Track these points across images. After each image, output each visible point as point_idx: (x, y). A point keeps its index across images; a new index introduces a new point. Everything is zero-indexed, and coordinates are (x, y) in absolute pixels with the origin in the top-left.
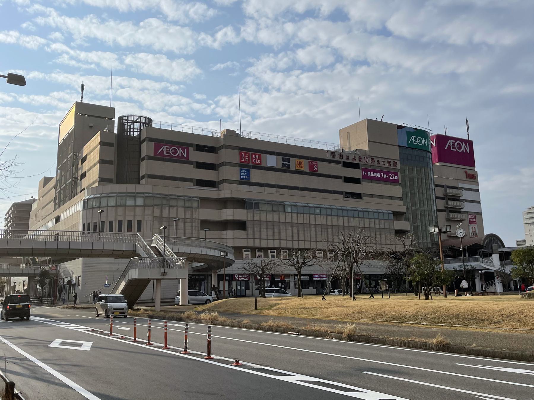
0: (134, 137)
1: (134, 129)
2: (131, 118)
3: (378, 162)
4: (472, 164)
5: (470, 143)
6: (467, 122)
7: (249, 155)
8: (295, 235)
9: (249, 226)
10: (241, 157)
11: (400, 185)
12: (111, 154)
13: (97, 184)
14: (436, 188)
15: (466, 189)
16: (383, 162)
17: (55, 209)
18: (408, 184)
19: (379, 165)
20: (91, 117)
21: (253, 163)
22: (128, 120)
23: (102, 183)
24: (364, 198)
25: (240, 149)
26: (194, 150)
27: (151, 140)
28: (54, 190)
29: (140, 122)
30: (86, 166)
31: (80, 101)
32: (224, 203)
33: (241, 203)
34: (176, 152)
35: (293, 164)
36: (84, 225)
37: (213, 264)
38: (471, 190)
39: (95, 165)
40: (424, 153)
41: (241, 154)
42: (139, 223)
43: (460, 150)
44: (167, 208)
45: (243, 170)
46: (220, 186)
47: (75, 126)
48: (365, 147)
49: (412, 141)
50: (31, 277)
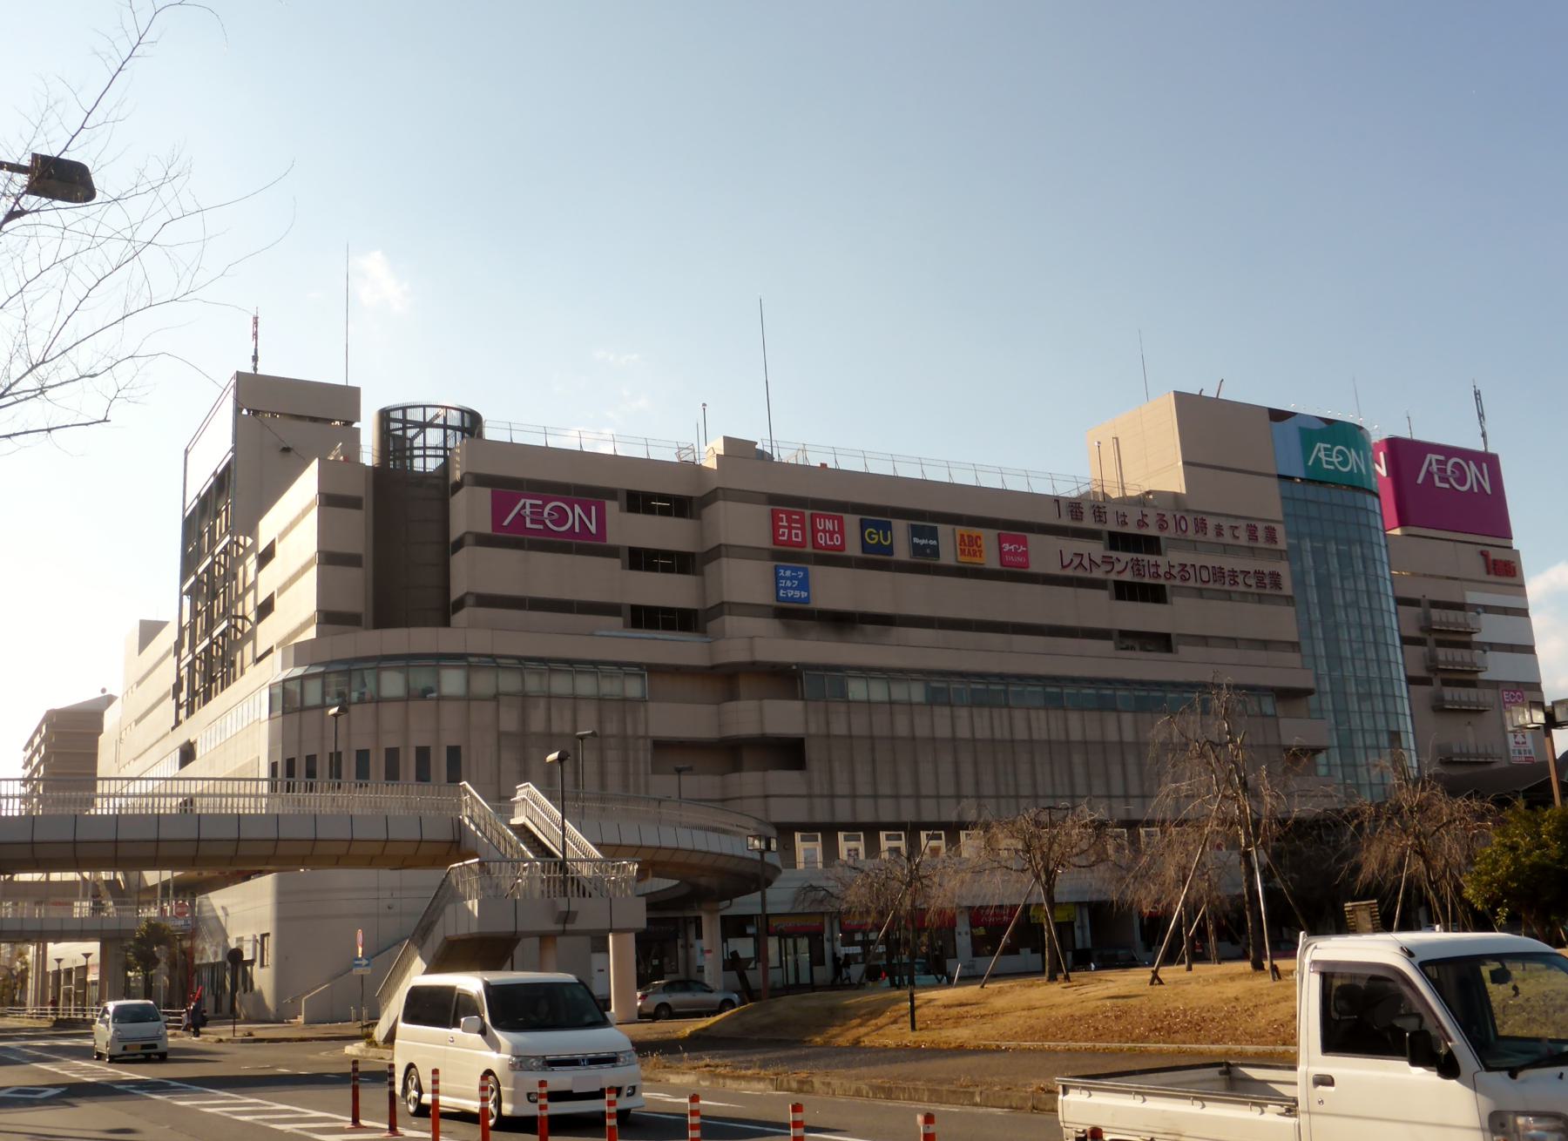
0: (425, 475)
1: (425, 448)
2: (415, 415)
3: (1219, 530)
4: (1502, 528)
5: (1489, 462)
6: (1477, 394)
7: (802, 521)
8: (1080, 780)
9: (813, 753)
10: (775, 528)
11: (1289, 600)
12: (356, 531)
13: (311, 633)
14: (1402, 608)
15: (1488, 609)
16: (1234, 528)
17: (178, 723)
18: (1313, 597)
19: (1221, 540)
20: (282, 421)
21: (815, 544)
22: (404, 421)
23: (329, 627)
24: (1181, 648)
25: (773, 499)
26: (621, 510)
27: (481, 480)
28: (172, 660)
29: (445, 427)
30: (269, 580)
31: (249, 369)
32: (727, 679)
33: (785, 679)
34: (563, 519)
35: (948, 544)
36: (274, 767)
37: (703, 881)
38: (1505, 611)
39: (304, 569)
40: (1359, 495)
41: (775, 519)
42: (454, 753)
43: (1463, 484)
44: (542, 703)
45: (786, 569)
46: (712, 626)
47: (233, 450)
48: (1173, 480)
49: (1318, 459)
50: (111, 940)
